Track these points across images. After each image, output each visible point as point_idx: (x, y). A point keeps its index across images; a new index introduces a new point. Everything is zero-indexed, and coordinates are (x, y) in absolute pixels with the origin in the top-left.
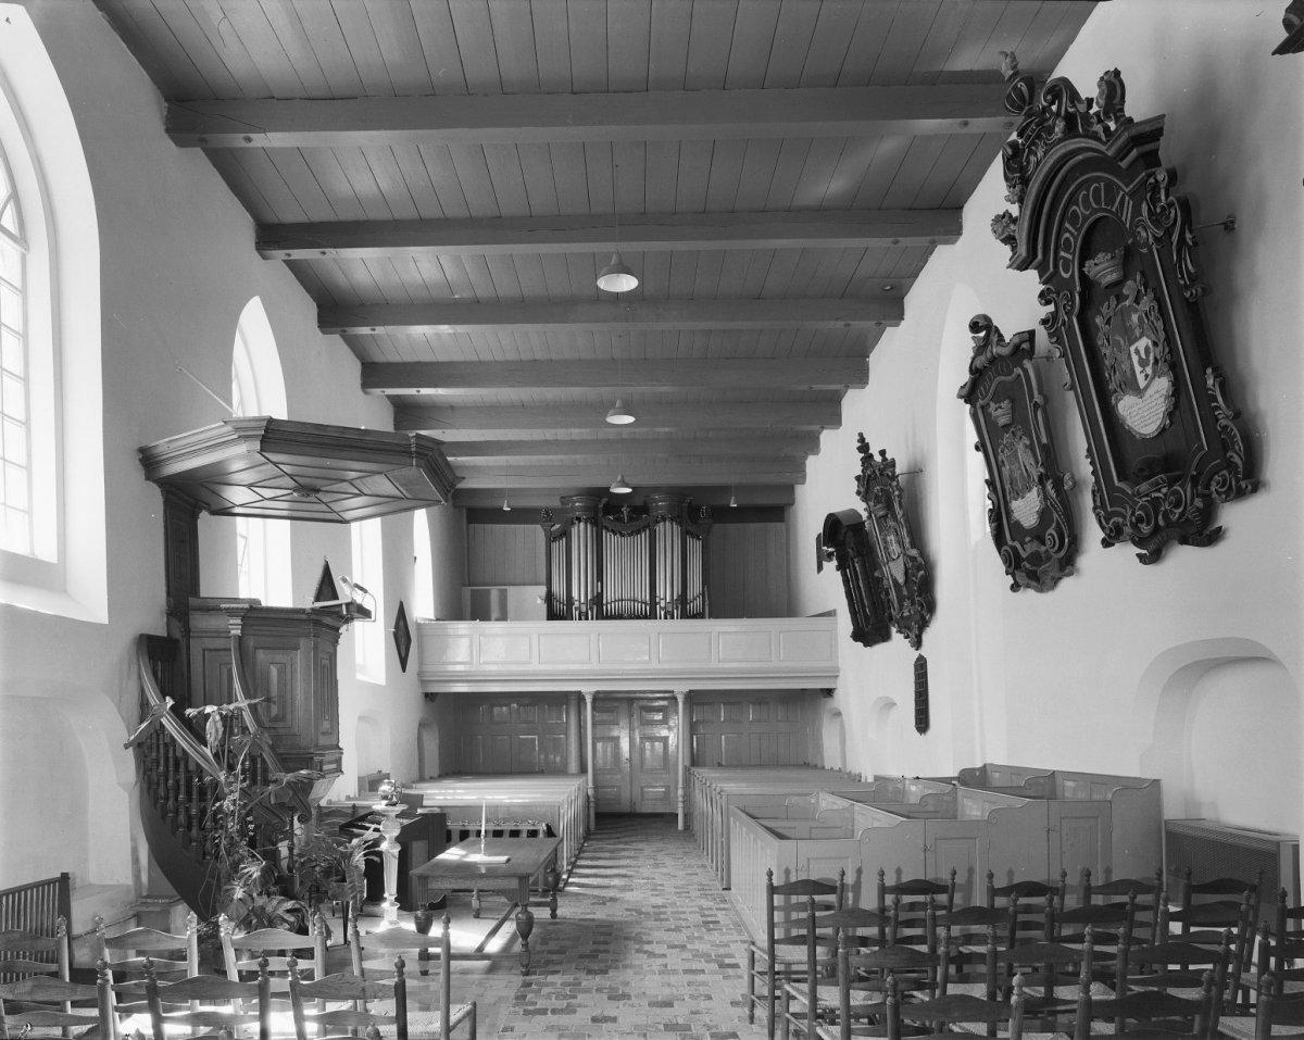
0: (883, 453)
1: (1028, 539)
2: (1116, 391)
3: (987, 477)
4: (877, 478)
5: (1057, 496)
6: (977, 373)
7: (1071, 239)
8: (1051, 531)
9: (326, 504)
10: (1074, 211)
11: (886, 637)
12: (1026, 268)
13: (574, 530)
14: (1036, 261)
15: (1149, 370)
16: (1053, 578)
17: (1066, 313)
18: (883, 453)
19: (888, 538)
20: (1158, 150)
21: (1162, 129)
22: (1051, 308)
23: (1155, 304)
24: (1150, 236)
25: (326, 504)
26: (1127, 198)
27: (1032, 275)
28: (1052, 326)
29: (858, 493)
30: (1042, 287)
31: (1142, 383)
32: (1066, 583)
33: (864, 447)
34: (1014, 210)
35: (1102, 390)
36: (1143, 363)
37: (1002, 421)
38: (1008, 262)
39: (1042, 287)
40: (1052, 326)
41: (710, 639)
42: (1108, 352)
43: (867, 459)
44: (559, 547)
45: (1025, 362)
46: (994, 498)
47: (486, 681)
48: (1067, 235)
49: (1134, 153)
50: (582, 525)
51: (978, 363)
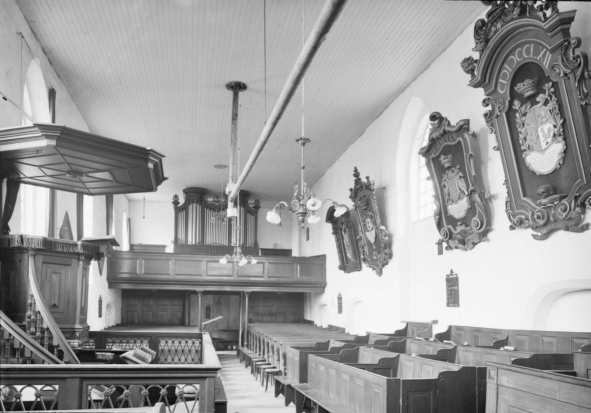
0: (367, 178)
1: (459, 223)
2: (525, 150)
3: (434, 194)
4: (363, 191)
5: (481, 201)
6: (433, 142)
7: (508, 73)
8: (476, 218)
9: (83, 183)
10: (512, 59)
11: (358, 268)
12: (478, 87)
13: (190, 207)
14: (485, 83)
15: (550, 140)
16: (473, 243)
17: (500, 111)
18: (367, 178)
19: (367, 220)
20: (569, 28)
21: (574, 17)
22: (490, 108)
23: (557, 106)
24: (561, 71)
25: (83, 183)
26: (548, 53)
27: (481, 90)
28: (490, 117)
29: (351, 197)
30: (486, 97)
31: (544, 146)
32: (481, 246)
33: (357, 174)
34: (476, 56)
35: (515, 151)
36: (546, 137)
37: (447, 165)
38: (469, 83)
39: (486, 97)
40: (490, 117)
41: (231, 276)
42: (523, 131)
43: (358, 181)
44: (182, 215)
45: (465, 134)
46: (438, 204)
47: (13, 329)
48: (505, 71)
49: (559, 28)
50: (194, 204)
51: (434, 136)
